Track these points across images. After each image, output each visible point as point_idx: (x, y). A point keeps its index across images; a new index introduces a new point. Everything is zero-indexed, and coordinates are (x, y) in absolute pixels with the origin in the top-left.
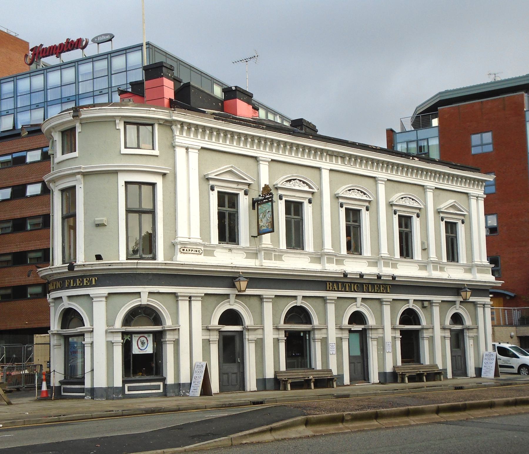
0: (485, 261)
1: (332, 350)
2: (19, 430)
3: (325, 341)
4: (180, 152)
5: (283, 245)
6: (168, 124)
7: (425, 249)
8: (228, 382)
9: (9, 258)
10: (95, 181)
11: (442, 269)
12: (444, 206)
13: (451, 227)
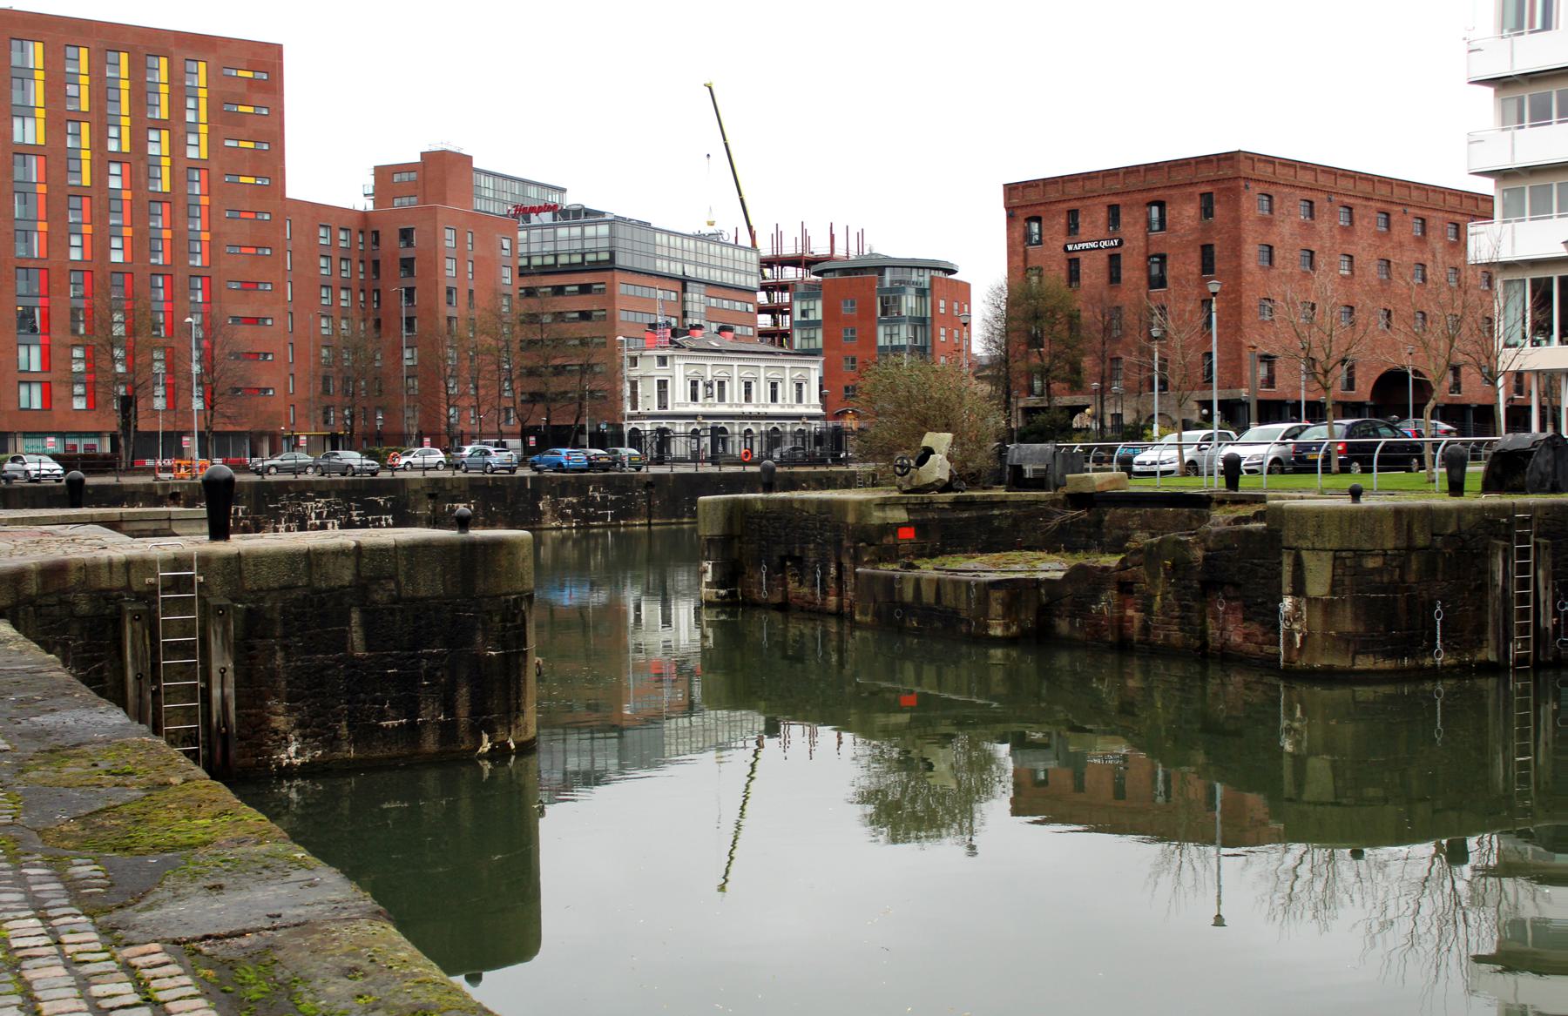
1: (737, 445)
2: (1110, 267)
3: (733, 442)
4: (677, 367)
5: (716, 401)
6: (672, 356)
7: (784, 398)
9: (576, 315)
10: (645, 380)
12: (794, 376)
13: (799, 386)
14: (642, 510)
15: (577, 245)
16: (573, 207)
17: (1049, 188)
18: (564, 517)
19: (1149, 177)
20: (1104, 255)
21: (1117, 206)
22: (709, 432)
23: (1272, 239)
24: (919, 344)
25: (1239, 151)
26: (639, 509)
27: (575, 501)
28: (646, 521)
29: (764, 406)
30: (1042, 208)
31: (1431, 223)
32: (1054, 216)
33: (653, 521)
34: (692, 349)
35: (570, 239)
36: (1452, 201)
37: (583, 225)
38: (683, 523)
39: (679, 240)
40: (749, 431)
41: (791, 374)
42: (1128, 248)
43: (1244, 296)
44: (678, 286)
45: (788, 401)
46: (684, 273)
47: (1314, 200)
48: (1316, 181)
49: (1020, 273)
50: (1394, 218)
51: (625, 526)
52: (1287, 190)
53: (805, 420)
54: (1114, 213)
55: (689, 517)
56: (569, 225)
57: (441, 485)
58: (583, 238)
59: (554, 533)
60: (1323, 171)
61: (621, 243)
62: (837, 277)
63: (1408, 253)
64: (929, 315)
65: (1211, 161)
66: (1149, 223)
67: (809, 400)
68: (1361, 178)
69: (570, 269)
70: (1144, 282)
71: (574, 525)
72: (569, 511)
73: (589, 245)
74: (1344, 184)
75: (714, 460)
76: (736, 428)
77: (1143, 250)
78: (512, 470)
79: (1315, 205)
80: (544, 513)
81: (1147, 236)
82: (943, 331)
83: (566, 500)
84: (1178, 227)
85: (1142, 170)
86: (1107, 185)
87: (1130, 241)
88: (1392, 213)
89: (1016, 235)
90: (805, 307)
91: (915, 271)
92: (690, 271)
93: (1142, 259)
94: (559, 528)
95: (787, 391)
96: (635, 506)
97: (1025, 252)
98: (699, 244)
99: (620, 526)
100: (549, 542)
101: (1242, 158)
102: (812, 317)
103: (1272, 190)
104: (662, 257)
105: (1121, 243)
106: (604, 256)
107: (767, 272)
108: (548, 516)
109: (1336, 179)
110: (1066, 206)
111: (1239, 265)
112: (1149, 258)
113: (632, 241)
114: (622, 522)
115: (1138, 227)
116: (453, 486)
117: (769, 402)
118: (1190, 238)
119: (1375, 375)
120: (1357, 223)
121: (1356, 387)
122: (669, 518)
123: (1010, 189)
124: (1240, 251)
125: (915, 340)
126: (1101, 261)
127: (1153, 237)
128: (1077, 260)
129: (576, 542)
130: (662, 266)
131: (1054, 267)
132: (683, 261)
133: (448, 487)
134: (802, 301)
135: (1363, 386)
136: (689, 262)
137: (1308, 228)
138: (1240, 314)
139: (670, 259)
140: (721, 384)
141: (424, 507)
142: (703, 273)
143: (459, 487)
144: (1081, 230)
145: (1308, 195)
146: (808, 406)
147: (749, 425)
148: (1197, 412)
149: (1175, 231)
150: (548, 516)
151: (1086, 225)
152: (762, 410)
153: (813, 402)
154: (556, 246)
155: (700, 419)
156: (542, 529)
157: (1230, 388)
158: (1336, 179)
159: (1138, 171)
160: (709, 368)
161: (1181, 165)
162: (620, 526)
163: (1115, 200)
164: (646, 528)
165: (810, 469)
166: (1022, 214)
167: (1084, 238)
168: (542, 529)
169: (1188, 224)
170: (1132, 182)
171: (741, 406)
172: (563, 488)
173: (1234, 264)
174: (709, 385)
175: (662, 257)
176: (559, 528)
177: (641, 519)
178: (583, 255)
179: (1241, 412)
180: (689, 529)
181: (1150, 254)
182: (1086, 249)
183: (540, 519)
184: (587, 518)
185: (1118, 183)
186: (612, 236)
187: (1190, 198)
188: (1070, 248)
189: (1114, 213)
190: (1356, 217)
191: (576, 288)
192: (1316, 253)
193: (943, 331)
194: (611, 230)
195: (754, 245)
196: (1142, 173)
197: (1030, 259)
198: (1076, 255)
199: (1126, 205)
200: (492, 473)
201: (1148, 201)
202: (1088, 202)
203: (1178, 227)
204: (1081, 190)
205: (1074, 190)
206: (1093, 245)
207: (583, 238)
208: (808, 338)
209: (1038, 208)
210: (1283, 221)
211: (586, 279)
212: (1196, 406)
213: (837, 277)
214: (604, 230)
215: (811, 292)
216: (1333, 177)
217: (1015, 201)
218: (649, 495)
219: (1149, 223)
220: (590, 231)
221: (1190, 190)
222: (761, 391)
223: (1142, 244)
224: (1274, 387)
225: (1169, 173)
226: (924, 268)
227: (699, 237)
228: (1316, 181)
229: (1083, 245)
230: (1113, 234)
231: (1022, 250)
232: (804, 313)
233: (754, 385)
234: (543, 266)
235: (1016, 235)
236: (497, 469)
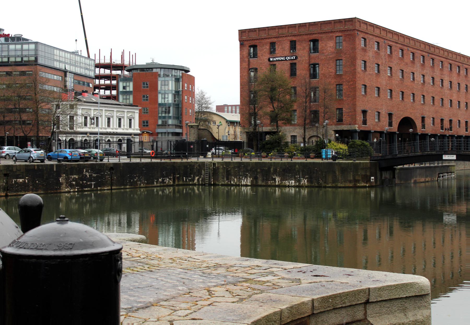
0: (138, 128)
5: (95, 126)
7: (124, 126)
8: (460, 234)
11: (128, 130)
12: (128, 116)
13: (130, 120)
14: (108, 182)
15: (19, 53)
16: (17, 36)
17: (261, 32)
18: (71, 186)
19: (311, 28)
20: (288, 63)
21: (295, 42)
22: (126, 142)
23: (366, 58)
24: (176, 103)
25: (355, 18)
26: (107, 182)
27: (77, 177)
28: (110, 188)
29: (104, 128)
30: (258, 41)
31: (416, 55)
32: (263, 45)
33: (113, 188)
34: (85, 102)
35: (16, 50)
36: (423, 46)
37: (22, 44)
38: (127, 188)
39: (63, 53)
40: (109, 140)
41: (127, 114)
42: (300, 60)
43: (357, 83)
44: (63, 74)
45: (126, 127)
46: (65, 68)
47: (379, 42)
48: (380, 33)
49: (246, 71)
50: (405, 52)
51: (100, 190)
52: (371, 37)
53: (133, 136)
54: (293, 46)
55: (129, 185)
56: (15, 44)
57: (11, 169)
58: (22, 50)
59: (66, 195)
60: (383, 30)
61: (40, 53)
62: (139, 72)
63: (409, 68)
64: (181, 89)
65: (342, 22)
66: (249, 54)
67: (134, 126)
68: (395, 34)
69: (17, 64)
70: (308, 76)
71: (76, 190)
72: (74, 183)
73: (25, 53)
74: (389, 36)
75: (129, 154)
76: (137, 139)
77: (308, 61)
78: (42, 161)
79: (380, 44)
80: (62, 184)
81: (309, 55)
82: (186, 97)
83: (73, 177)
84: (325, 51)
85: (307, 25)
86: (290, 31)
87: (301, 57)
88: (404, 50)
89: (245, 53)
90: (125, 85)
91: (173, 70)
92: (68, 68)
93: (307, 65)
94: (69, 192)
95: (125, 122)
96: (105, 179)
97: (249, 61)
98: (71, 55)
99: (98, 190)
100: (64, 199)
101: (357, 21)
102: (128, 89)
103: (366, 36)
104: (57, 61)
105: (296, 58)
106: (33, 59)
107: (97, 70)
108: (64, 186)
109: (387, 33)
110: (290, 38)
111: (355, 69)
112: (310, 65)
113: (45, 52)
114: (99, 188)
115: (305, 51)
116: (17, 169)
117: (118, 127)
118: (331, 56)
119: (399, 120)
120: (393, 53)
121: (393, 125)
122: (121, 185)
123: (242, 32)
124: (355, 63)
125: (175, 101)
126: (287, 66)
127: (312, 56)
128: (275, 65)
129: (77, 199)
130: (57, 65)
131: (263, 68)
132: (65, 63)
133: (15, 170)
134: (123, 82)
135: (395, 125)
136: (67, 63)
137: (377, 54)
138: (355, 91)
139: (60, 62)
140: (97, 118)
141: (2, 181)
142: (73, 69)
143: (20, 170)
144: (277, 52)
145: (378, 40)
146: (134, 130)
147: (109, 138)
148: (334, 135)
149: (323, 53)
150: (64, 186)
151: (279, 49)
152: (115, 131)
153: (136, 128)
154: (8, 53)
155: (88, 134)
156: (61, 193)
157: (350, 124)
158: (387, 33)
159: (306, 26)
160: (92, 111)
161: (327, 23)
162: (98, 190)
163: (294, 39)
164: (109, 191)
165: (158, 161)
166: (247, 44)
167: (278, 55)
168: (61, 193)
169: (330, 50)
170: (302, 30)
171: (106, 129)
172: (71, 170)
173: (352, 69)
174: (91, 119)
175: (57, 61)
176: (69, 192)
177: (107, 187)
178: (9, 58)
179: (355, 135)
180: (129, 191)
181: (250, 67)
182: (279, 60)
183: (60, 187)
184: (83, 186)
185: (296, 31)
186: (36, 50)
187: (331, 38)
188: (271, 59)
189: (293, 46)
190: (393, 50)
191: (5, 73)
192: (380, 65)
193: (186, 97)
194: (36, 47)
195: (89, 56)
196: (307, 26)
197: (251, 64)
198: (274, 63)
199: (299, 41)
200: (33, 162)
201: (310, 39)
202: (280, 39)
203: (325, 51)
204: (277, 33)
205: (274, 33)
206: (283, 59)
207: (22, 50)
208: (126, 99)
209: (256, 41)
210: (369, 50)
211: (23, 69)
212: (333, 133)
213: (139, 72)
214: (32, 47)
215: (126, 79)
216: (386, 32)
217: (244, 38)
218: (111, 174)
219: (249, 54)
220: (25, 47)
221: (331, 35)
222: (115, 122)
223: (307, 59)
224: (366, 125)
225: (321, 27)
226: (177, 69)
227: (73, 53)
228: (380, 33)
229: (278, 59)
230: (293, 54)
231: (247, 60)
232: (124, 88)
233: (111, 119)
234: (16, 62)
235: (245, 53)
236: (35, 160)
